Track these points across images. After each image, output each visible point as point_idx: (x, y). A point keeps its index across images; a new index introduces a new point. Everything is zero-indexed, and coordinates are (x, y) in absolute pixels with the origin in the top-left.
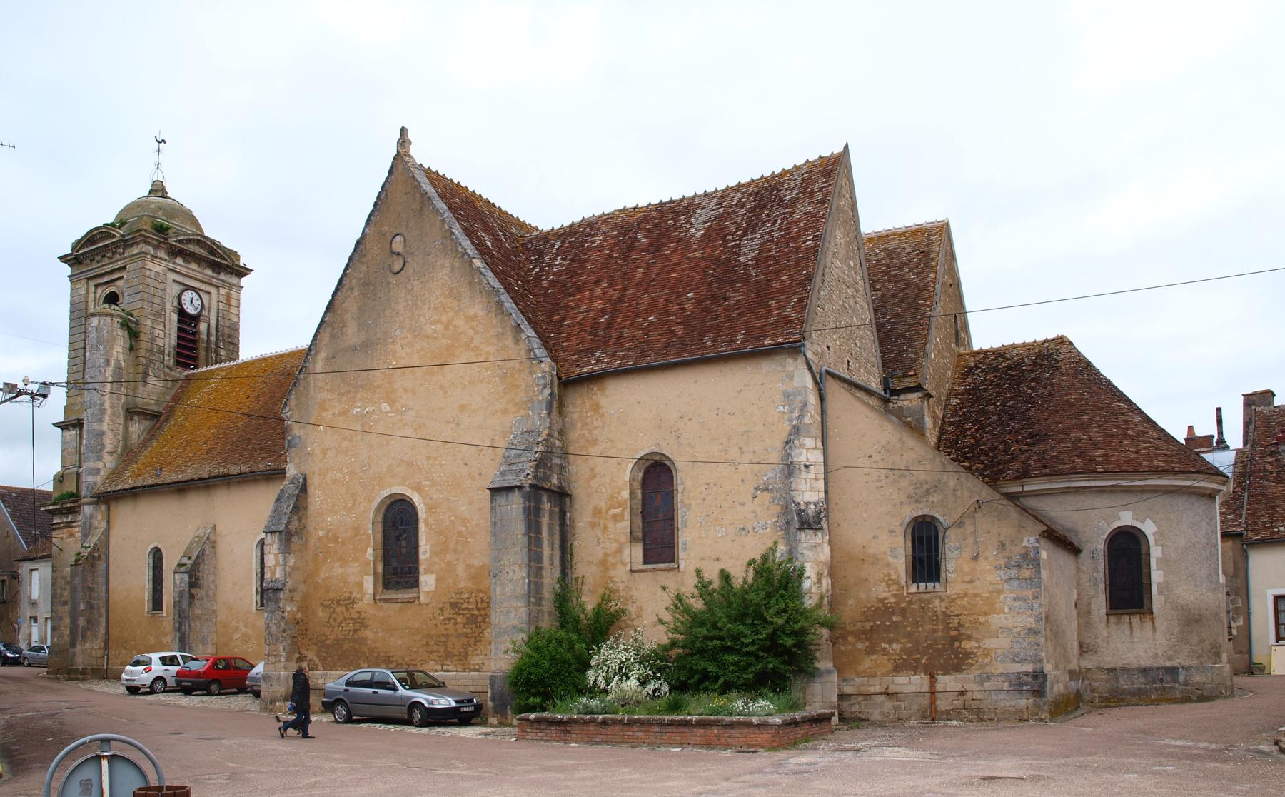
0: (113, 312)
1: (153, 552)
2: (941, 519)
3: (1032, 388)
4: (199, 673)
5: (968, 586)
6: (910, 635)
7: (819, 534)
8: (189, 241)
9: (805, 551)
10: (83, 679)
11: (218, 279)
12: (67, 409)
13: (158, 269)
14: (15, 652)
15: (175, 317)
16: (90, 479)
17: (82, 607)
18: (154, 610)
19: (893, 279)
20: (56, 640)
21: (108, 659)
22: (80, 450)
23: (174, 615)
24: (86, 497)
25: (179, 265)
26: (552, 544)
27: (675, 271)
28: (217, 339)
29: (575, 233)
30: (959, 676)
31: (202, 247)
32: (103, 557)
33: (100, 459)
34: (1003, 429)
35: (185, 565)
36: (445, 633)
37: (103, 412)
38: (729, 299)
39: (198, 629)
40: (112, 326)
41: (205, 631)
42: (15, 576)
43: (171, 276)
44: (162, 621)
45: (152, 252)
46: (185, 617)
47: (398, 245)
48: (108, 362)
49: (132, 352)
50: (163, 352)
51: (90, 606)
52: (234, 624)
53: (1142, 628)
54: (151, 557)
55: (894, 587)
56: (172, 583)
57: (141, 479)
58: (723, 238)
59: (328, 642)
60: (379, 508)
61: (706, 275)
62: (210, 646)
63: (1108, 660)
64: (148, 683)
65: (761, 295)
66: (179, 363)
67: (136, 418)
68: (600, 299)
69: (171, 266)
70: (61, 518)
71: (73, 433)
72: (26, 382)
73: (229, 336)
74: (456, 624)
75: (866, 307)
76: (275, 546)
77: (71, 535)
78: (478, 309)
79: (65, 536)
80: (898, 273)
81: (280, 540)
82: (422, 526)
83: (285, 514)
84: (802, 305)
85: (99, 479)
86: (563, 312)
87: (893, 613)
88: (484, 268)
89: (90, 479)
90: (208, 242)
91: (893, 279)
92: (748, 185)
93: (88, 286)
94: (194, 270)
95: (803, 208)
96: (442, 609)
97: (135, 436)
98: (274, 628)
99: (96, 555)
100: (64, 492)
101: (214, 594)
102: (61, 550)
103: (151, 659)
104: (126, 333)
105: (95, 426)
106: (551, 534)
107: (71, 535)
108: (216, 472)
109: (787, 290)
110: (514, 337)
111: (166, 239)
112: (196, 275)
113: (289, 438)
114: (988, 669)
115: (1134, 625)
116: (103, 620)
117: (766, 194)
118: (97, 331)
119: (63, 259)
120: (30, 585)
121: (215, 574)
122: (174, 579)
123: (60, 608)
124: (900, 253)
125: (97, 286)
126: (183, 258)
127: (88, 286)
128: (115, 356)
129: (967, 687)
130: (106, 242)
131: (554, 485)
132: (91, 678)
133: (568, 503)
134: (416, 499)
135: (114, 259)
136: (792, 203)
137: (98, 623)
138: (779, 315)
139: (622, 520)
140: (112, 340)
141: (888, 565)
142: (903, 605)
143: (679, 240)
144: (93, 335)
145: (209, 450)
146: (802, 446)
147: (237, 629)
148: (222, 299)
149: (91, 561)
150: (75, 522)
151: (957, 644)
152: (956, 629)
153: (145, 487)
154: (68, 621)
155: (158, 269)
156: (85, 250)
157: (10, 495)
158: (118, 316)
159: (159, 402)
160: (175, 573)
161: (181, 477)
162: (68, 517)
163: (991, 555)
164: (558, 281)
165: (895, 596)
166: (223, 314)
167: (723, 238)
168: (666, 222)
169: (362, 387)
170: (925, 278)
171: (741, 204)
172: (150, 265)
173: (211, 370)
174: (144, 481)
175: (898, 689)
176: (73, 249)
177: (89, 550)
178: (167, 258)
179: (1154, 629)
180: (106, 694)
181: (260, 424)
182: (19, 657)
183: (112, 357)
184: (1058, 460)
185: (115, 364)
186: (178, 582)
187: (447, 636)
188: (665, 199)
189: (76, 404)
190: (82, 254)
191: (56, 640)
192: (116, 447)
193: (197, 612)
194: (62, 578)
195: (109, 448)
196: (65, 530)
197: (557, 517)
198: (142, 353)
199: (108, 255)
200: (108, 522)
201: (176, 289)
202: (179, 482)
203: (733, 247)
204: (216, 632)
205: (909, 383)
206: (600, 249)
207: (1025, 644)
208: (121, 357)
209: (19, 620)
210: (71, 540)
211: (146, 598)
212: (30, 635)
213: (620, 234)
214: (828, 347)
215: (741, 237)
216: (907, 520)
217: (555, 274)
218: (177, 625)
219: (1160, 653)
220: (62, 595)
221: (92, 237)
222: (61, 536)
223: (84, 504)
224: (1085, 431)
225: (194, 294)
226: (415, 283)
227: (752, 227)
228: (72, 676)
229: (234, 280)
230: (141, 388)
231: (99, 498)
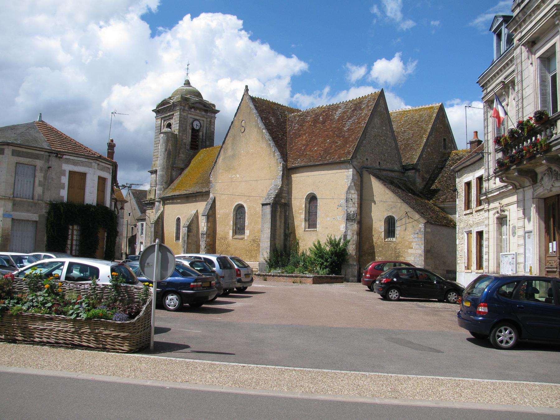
11: (207, 115)
15: (190, 131)
26: (281, 222)
27: (327, 132)
36: (251, 249)
38: (337, 143)
43: (190, 116)
56: (183, 231)
72: (127, 184)
74: (254, 246)
78: (264, 145)
79: (150, 212)
82: (246, 214)
88: (266, 132)
92: (355, 101)
96: (250, 241)
106: (280, 218)
107: (152, 212)
110: (273, 155)
128: (168, 148)
131: (283, 202)
133: (288, 208)
134: (245, 206)
139: (302, 214)
142: (383, 245)
143: (331, 120)
148: (208, 123)
152: (398, 253)
161: (187, 192)
163: (410, 229)
171: (351, 108)
176: (157, 108)
186: (184, 230)
187: (251, 250)
196: (150, 210)
201: (191, 120)
206: (309, 121)
207: (418, 260)
208: (171, 148)
210: (152, 214)
214: (367, 159)
215: (347, 120)
216: (385, 217)
220: (149, 234)
221: (164, 103)
226: (247, 136)
229: (213, 115)
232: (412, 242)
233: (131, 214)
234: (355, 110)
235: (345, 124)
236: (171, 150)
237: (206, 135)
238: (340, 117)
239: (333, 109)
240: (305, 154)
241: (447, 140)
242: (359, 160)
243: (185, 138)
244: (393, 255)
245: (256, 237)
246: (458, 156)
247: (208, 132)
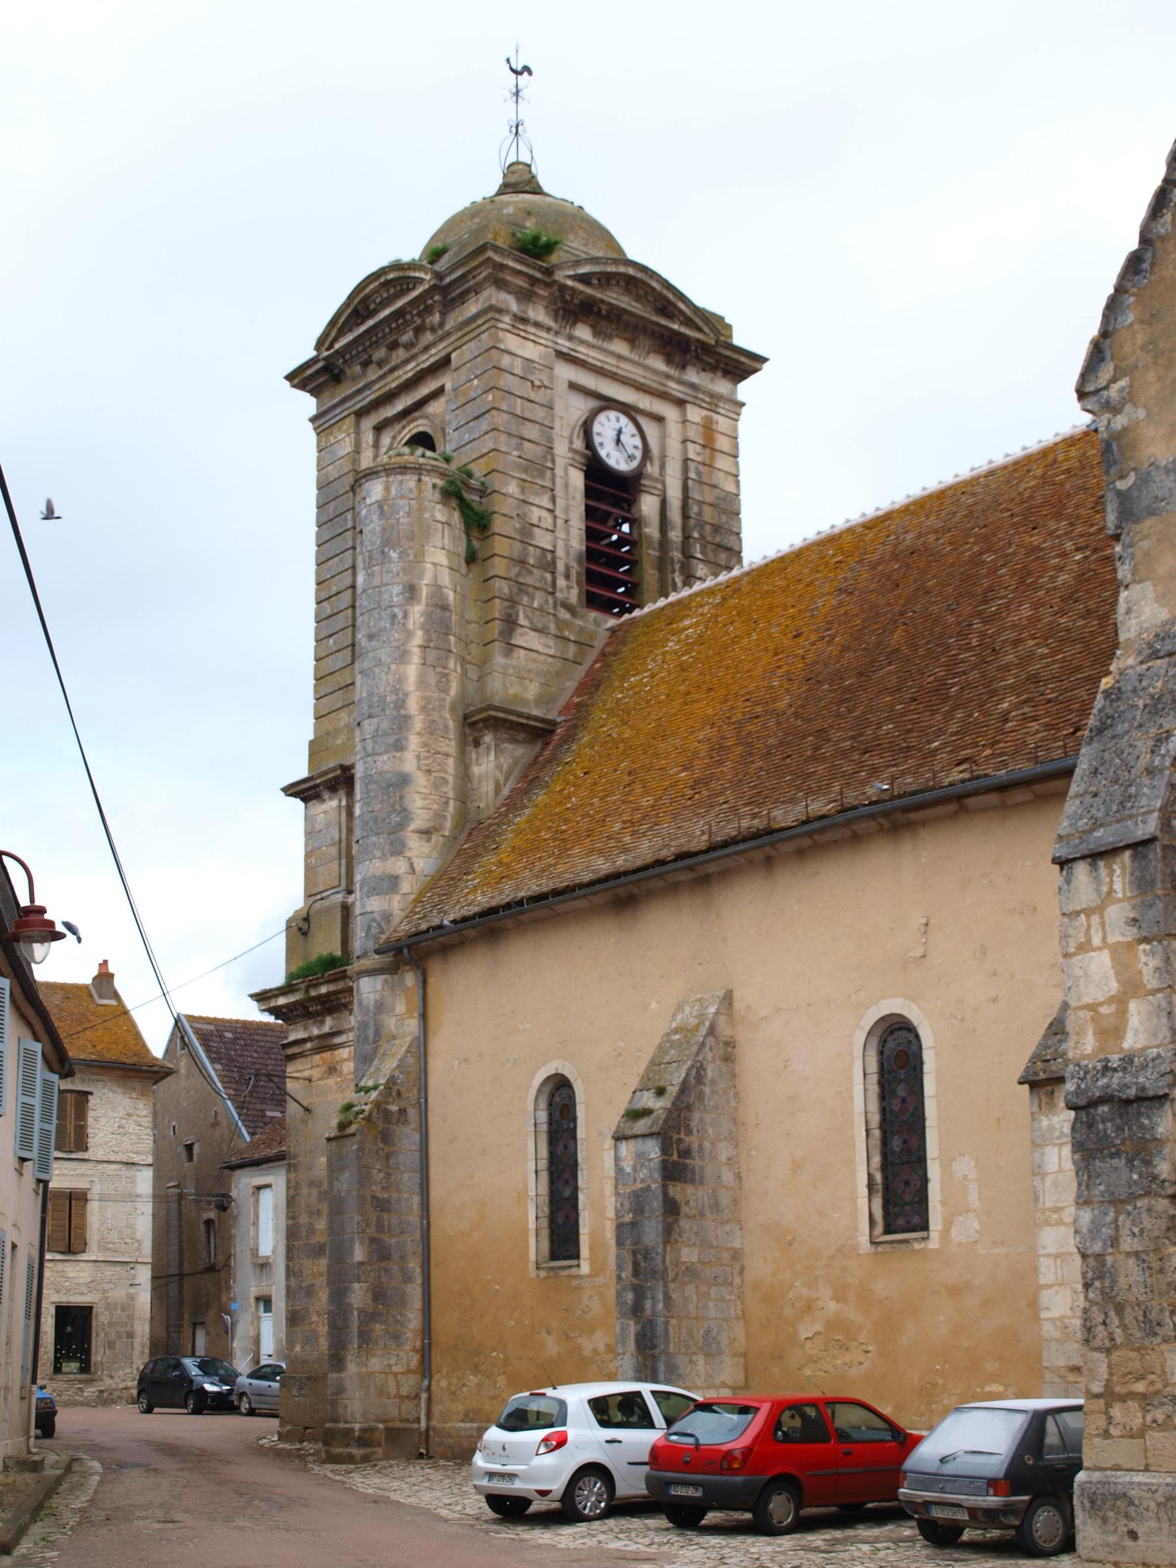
0: (421, 460)
1: (547, 1090)
4: (728, 1454)
8: (606, 280)
10: (366, 1459)
11: (680, 382)
12: (316, 749)
13: (531, 351)
14: (223, 1381)
15: (577, 479)
16: (375, 904)
17: (359, 1254)
18: (554, 1256)
20: (298, 1348)
21: (429, 1401)
22: (349, 847)
23: (620, 1267)
24: (365, 955)
25: (582, 342)
28: (686, 537)
31: (638, 298)
32: (412, 1113)
33: (398, 848)
35: (647, 1112)
37: (402, 722)
39: (692, 1307)
40: (419, 498)
41: (712, 1314)
42: (224, 1204)
43: (566, 373)
44: (578, 1288)
45: (514, 306)
46: (654, 1272)
48: (411, 591)
49: (472, 567)
50: (551, 567)
51: (381, 1253)
52: (800, 1290)
54: (543, 1104)
62: (727, 1360)
64: (558, 1485)
66: (593, 601)
67: (488, 738)
69: (564, 344)
70: (306, 1028)
71: (331, 804)
73: (717, 529)
76: (1117, 913)
77: (332, 1070)
79: (316, 1073)
81: (1142, 884)
83: (1150, 771)
85: (396, 904)
89: (375, 904)
90: (654, 284)
93: (358, 431)
94: (620, 357)
97: (488, 788)
98: (1130, 1275)
99: (394, 1108)
100: (314, 957)
101: (735, 1201)
102: (307, 1110)
103: (562, 1404)
104: (456, 515)
105: (385, 763)
107: (332, 1070)
108: (730, 830)
111: (549, 272)
112: (626, 370)
113: (1121, 485)
116: (415, 1291)
118: (382, 512)
120: (256, 1224)
121: (735, 1141)
122: (617, 1159)
123: (307, 1263)
125: (379, 429)
126: (593, 327)
127: (358, 431)
130: (399, 304)
132: (387, 1457)
135: (421, 346)
137: (403, 1302)
140: (420, 533)
144: (373, 526)
145: (696, 785)
147: (809, 1307)
148: (693, 433)
149: (381, 1124)
150: (339, 1033)
153: (520, 903)
154: (324, 1296)
155: (531, 351)
156: (349, 337)
157: (221, 1036)
158: (434, 470)
159: (541, 700)
160: (619, 1138)
161: (622, 862)
162: (322, 1022)
166: (698, 473)
172: (511, 342)
173: (679, 602)
174: (518, 889)
176: (318, 347)
177: (374, 1095)
178: (552, 324)
180: (427, 1514)
181: (848, 689)
182: (230, 1392)
183: (421, 575)
185: (431, 596)
189: (337, 732)
190: (340, 353)
191: (298, 1348)
192: (440, 816)
193: (689, 1255)
194: (312, 1184)
195: (420, 818)
196: (317, 1059)
198: (499, 566)
199: (407, 337)
200: (424, 1017)
201: (580, 406)
202: (616, 876)
204: (744, 1316)
208: (446, 579)
209: (234, 1306)
210: (331, 1081)
211: (532, 1225)
212: (257, 1341)
218: (630, 1296)
220: (311, 1230)
222: (306, 1074)
223: (362, 973)
225: (624, 420)
228: (337, 1450)
229: (721, 386)
230: (499, 660)
231: (398, 951)
233: (196, 1149)
236: (451, 596)
237: (685, 516)
243: (548, 522)
247: (695, 494)
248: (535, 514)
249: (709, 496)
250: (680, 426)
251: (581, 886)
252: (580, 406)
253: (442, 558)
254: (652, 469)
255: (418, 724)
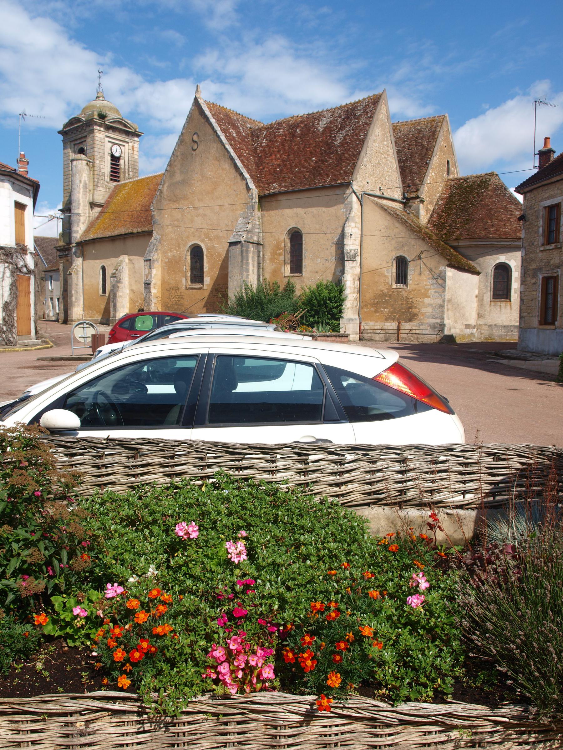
2: (407, 258)
3: (474, 197)
5: (417, 286)
6: (392, 305)
7: (355, 262)
8: (115, 122)
9: (349, 270)
15: (109, 158)
19: (417, 144)
27: (309, 148)
29: (272, 128)
30: (410, 323)
34: (457, 216)
38: (327, 161)
43: (107, 139)
47: (195, 138)
53: (505, 307)
55: (387, 286)
57: (96, 235)
58: (330, 133)
59: (169, 305)
60: (190, 247)
61: (321, 150)
63: (489, 322)
65: (340, 159)
66: (111, 180)
68: (279, 159)
69: (107, 134)
75: (394, 161)
80: (420, 141)
82: (205, 257)
84: (354, 166)
86: (264, 165)
87: (386, 296)
91: (417, 144)
92: (344, 106)
95: (363, 120)
106: (253, 261)
109: (349, 159)
114: (422, 321)
115: (502, 306)
117: (350, 111)
119: (60, 132)
124: (422, 131)
125: (75, 145)
129: (414, 328)
130: (78, 124)
134: (203, 246)
136: (358, 118)
138: (345, 170)
141: (385, 276)
146: (349, 226)
148: (131, 148)
151: (410, 310)
152: (411, 304)
160: (111, 277)
161: (113, 234)
164: (264, 150)
165: (387, 289)
167: (330, 133)
168: (309, 124)
169: (181, 198)
170: (431, 144)
171: (340, 116)
175: (386, 328)
179: (511, 309)
184: (475, 232)
188: (311, 112)
197: (256, 253)
199: (80, 130)
202: (112, 236)
203: (333, 137)
205: (414, 195)
206: (282, 135)
207: (438, 311)
208: (86, 179)
213: (290, 129)
214: (368, 183)
215: (337, 132)
217: (262, 147)
219: (513, 319)
224: (491, 219)
227: (342, 128)
232: (430, 289)
234: (347, 118)
235: (335, 136)
236: (87, 182)
238: (325, 128)
239: (315, 119)
240: (283, 176)
241: (450, 163)
242: (359, 183)
244: (404, 306)
245: (219, 285)
246: (467, 183)
248: (102, 166)
249: (133, 159)
250: (106, 437)
251: (106, 237)
252: (111, 145)
253: (86, 175)
254: (123, 155)
255: (82, 204)
